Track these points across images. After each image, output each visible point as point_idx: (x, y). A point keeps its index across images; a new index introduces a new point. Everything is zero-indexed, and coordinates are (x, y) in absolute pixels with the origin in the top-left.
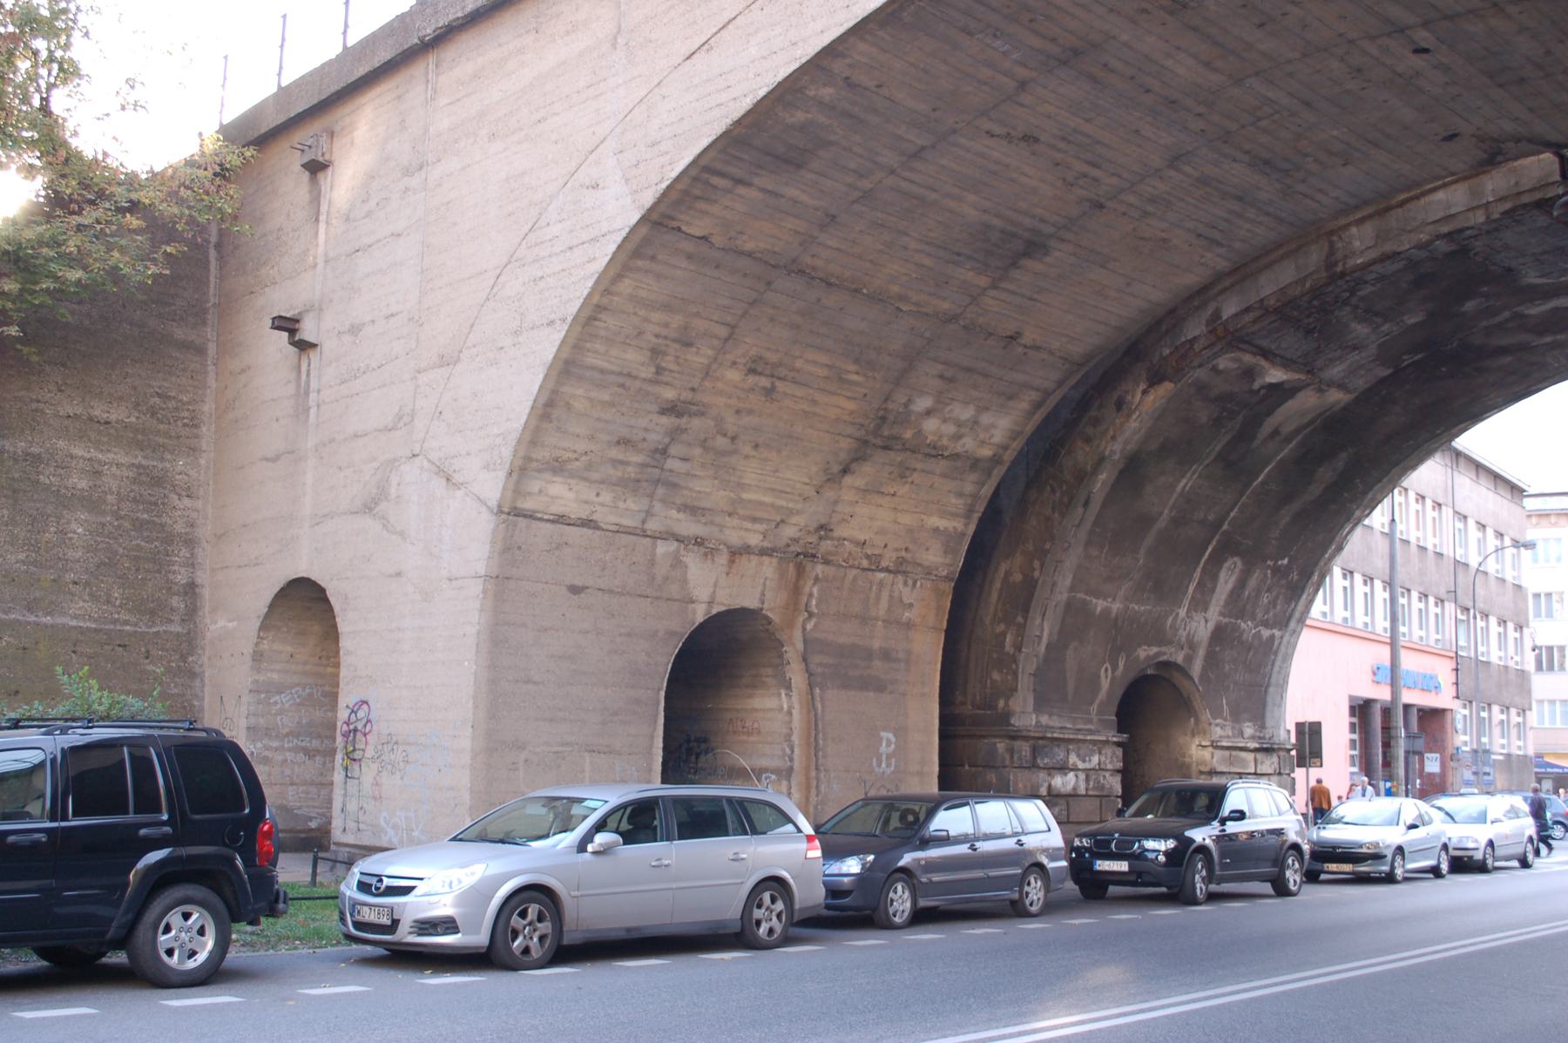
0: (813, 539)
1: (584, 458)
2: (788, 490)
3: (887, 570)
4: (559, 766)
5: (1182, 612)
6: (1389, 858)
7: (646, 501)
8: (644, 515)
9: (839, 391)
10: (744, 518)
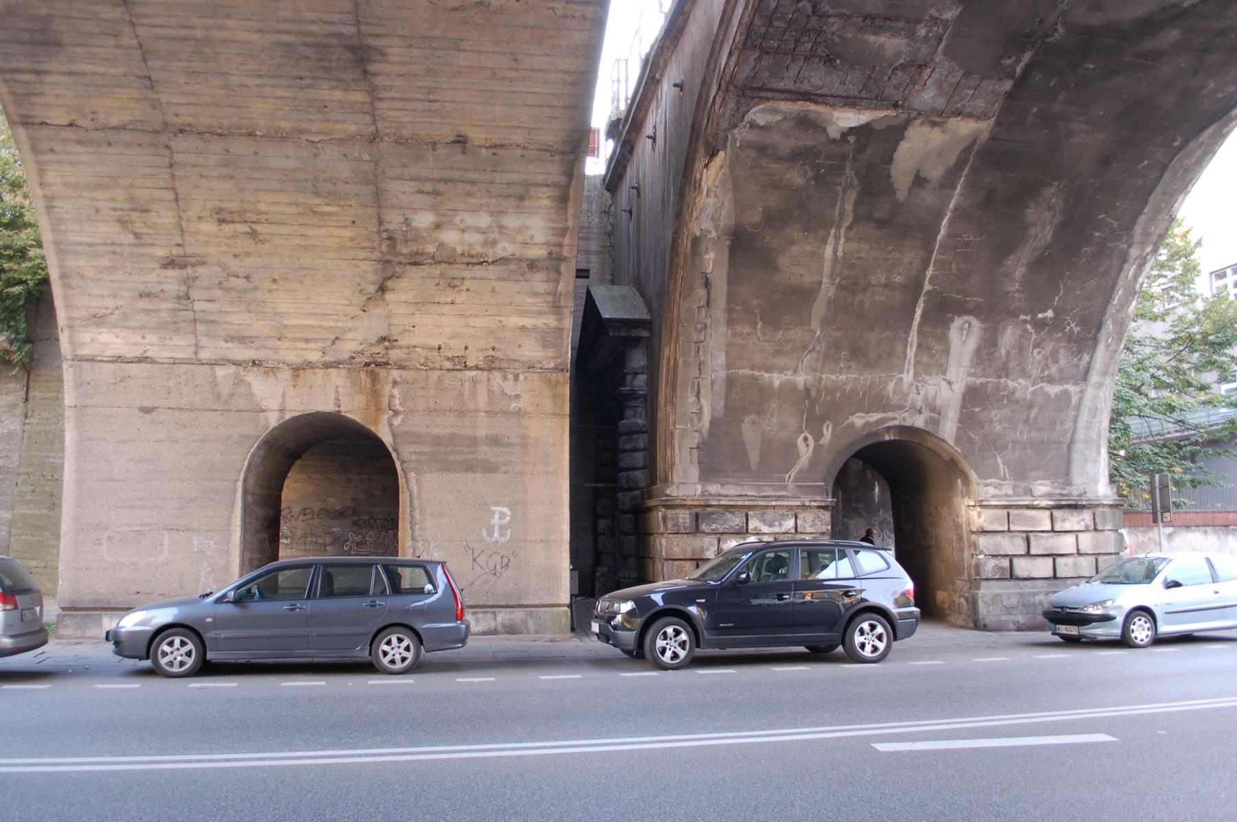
0: (380, 349)
1: (117, 312)
2: (331, 312)
3: (477, 368)
4: (139, 541)
5: (908, 377)
6: (1120, 619)
7: (190, 340)
8: (193, 348)
9: (323, 223)
10: (295, 340)
